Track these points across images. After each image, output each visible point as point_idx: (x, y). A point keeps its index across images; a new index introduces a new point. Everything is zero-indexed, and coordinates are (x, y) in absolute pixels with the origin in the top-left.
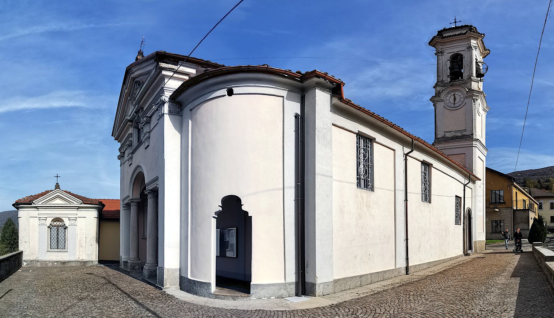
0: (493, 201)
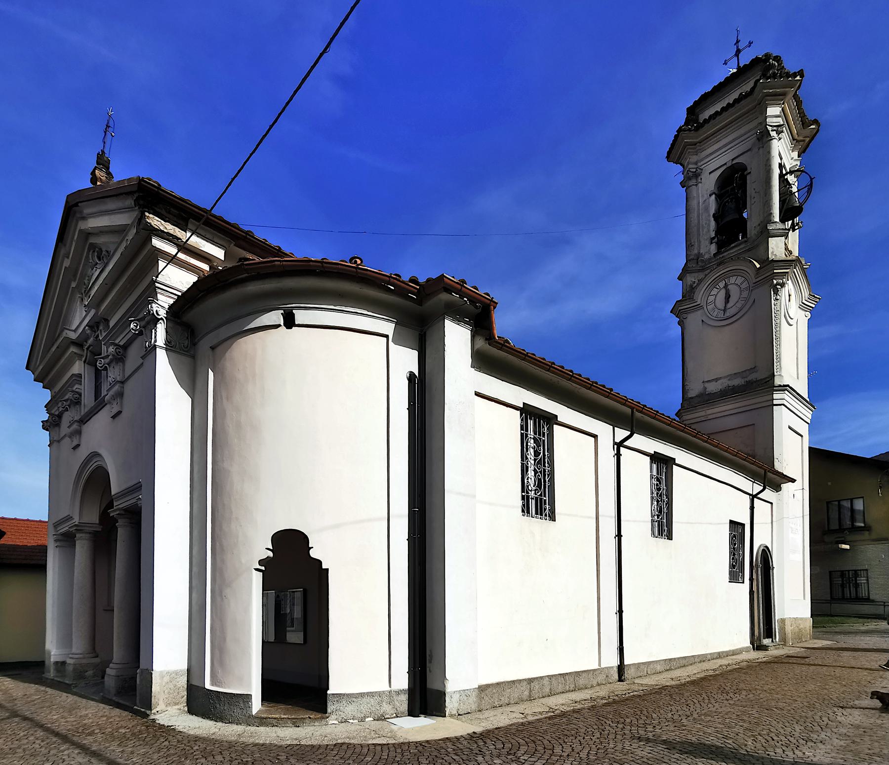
0: (835, 526)
